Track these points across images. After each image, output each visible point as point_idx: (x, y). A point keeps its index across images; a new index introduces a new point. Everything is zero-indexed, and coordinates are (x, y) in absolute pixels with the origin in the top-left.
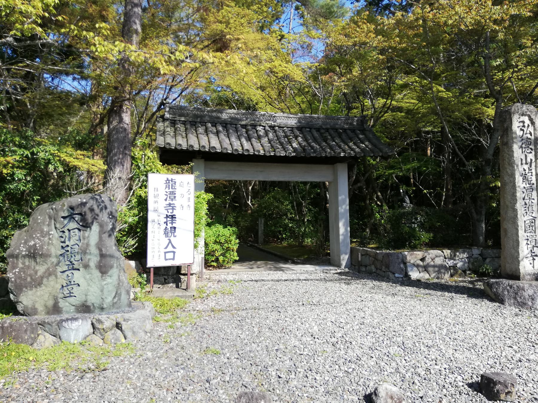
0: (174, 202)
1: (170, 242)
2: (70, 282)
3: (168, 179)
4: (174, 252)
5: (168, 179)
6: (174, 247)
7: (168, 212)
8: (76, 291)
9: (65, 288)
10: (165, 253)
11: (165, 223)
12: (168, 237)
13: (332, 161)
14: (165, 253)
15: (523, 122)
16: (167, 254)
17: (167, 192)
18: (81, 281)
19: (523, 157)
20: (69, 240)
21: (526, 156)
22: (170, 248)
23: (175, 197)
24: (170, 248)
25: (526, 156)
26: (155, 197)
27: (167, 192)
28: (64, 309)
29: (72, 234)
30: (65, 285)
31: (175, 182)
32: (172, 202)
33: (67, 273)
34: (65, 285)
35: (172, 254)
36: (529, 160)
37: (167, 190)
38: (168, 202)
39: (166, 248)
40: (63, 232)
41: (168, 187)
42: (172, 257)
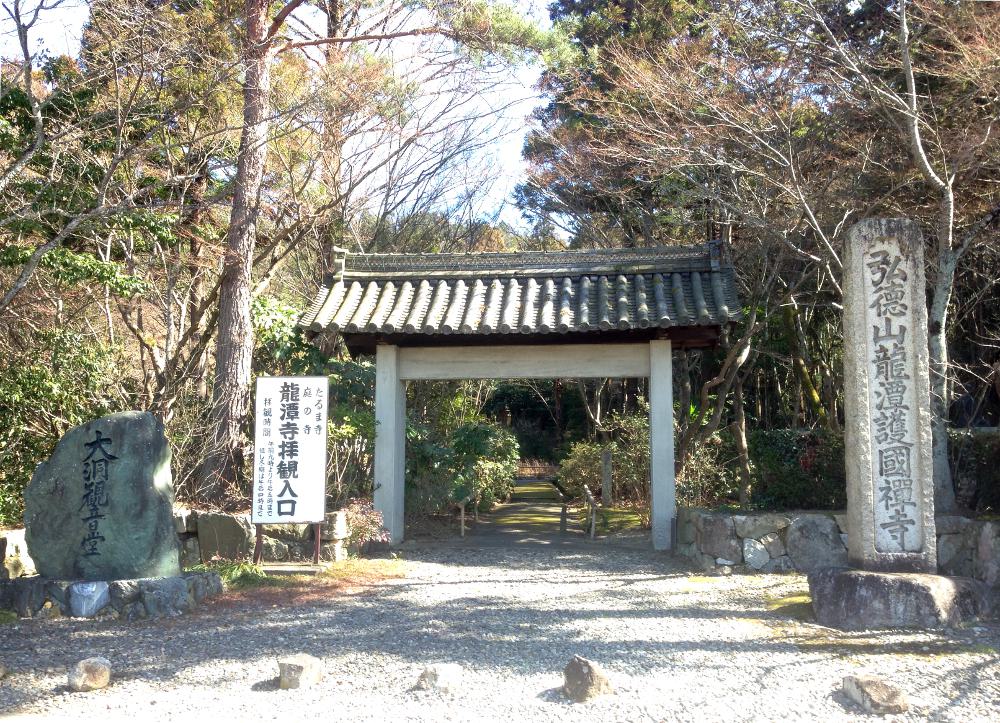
0: (295, 421)
1: (288, 485)
2: (93, 533)
3: (285, 383)
4: (293, 503)
5: (285, 383)
6: (294, 495)
7: (285, 437)
8: (100, 547)
9: (87, 543)
10: (280, 503)
11: (280, 454)
12: (284, 477)
13: (641, 336)
14: (280, 503)
15: (885, 254)
16: (290, 510)
17: (283, 405)
18: (107, 533)
19: (881, 323)
20: (94, 477)
21: (888, 321)
22: (287, 496)
23: (297, 413)
24: (287, 496)
25: (888, 321)
26: (266, 414)
27: (283, 405)
28: (86, 571)
29: (98, 467)
30: (87, 537)
31: (298, 389)
32: (291, 422)
33: (90, 521)
34: (87, 537)
35: (290, 505)
36: (895, 330)
37: (284, 402)
38: (285, 422)
39: (281, 495)
40: (87, 464)
41: (285, 396)
42: (290, 510)
